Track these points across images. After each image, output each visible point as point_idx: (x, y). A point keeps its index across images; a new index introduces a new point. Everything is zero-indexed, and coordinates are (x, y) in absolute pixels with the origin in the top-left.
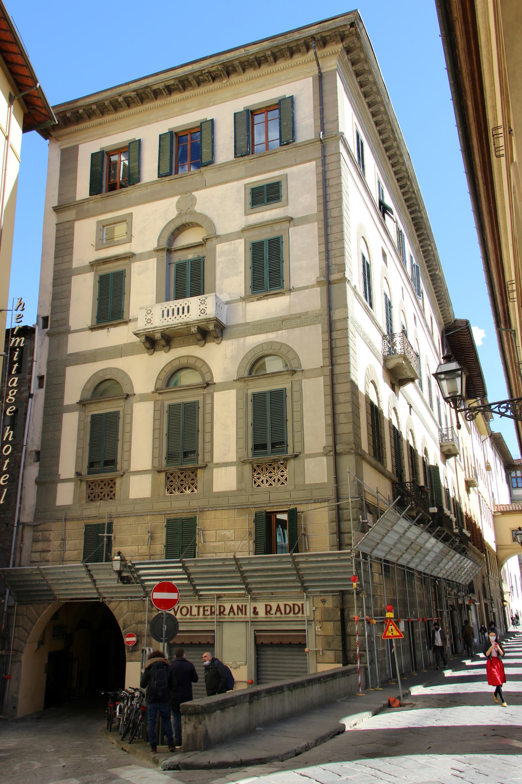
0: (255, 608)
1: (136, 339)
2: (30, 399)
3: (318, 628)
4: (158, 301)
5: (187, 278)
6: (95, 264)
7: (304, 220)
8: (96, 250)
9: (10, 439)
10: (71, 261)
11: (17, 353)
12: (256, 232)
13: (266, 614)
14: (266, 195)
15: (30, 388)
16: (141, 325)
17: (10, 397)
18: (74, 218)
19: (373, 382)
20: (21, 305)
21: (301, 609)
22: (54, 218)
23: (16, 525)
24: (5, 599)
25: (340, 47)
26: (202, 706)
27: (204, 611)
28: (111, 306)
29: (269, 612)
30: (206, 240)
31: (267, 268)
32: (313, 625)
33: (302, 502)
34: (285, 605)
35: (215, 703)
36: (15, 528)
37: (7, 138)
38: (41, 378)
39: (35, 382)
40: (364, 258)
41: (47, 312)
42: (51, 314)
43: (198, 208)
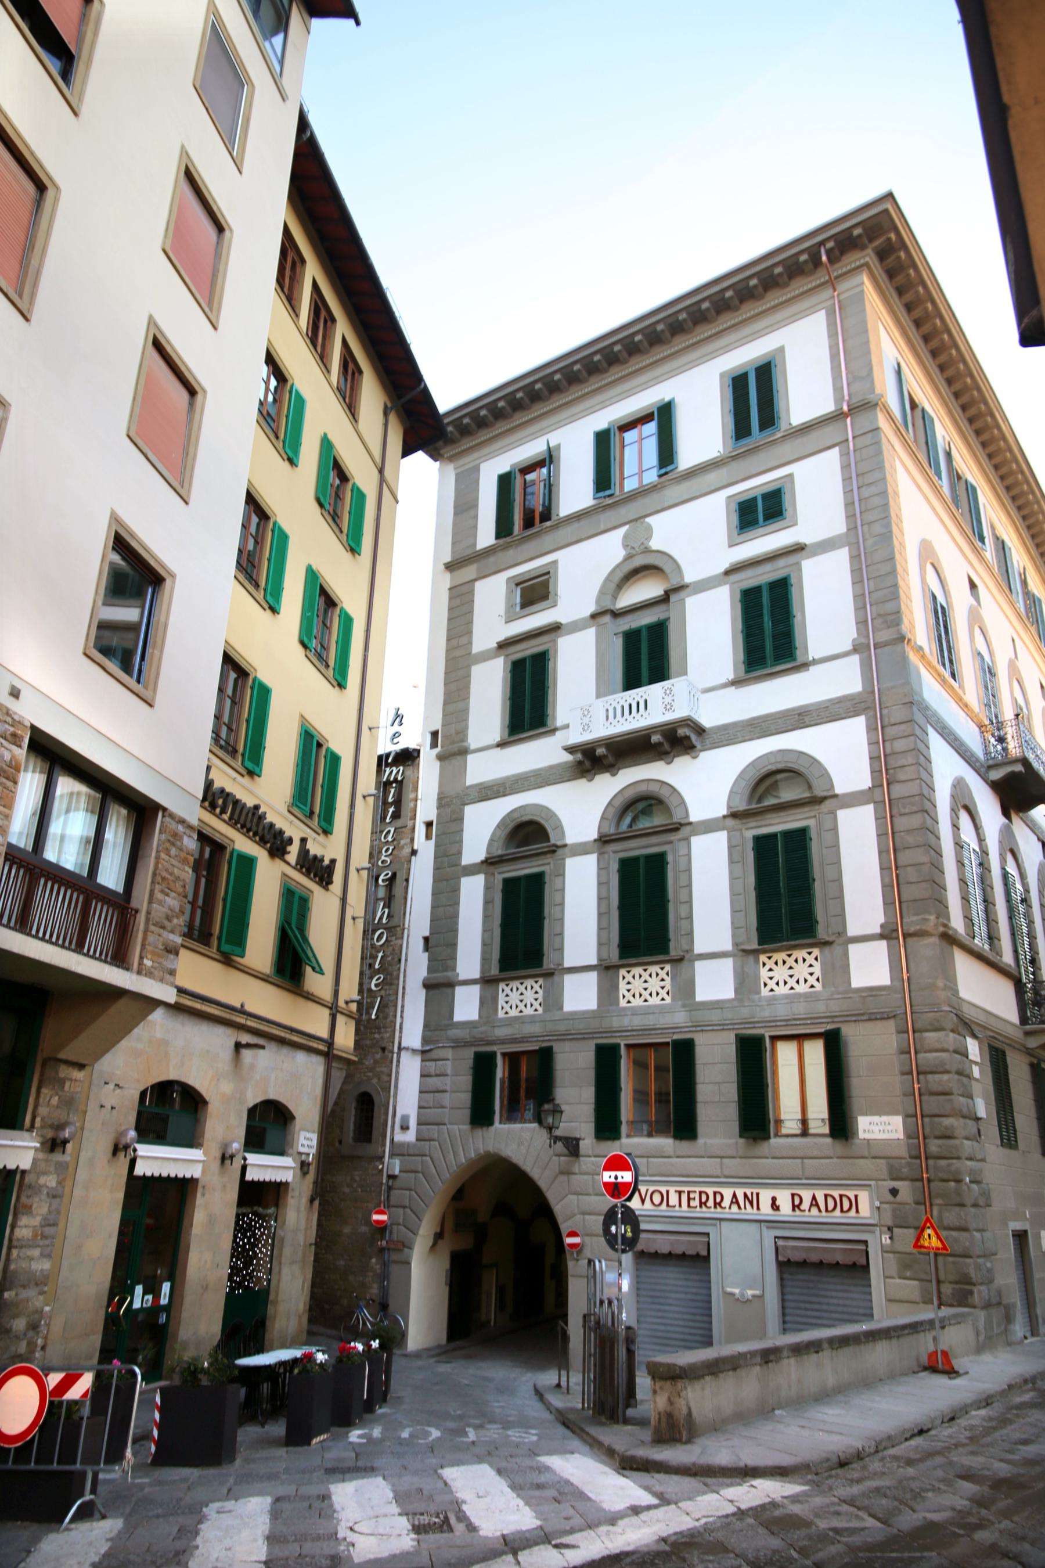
0: (774, 1199)
1: (568, 757)
2: (413, 858)
3: (886, 1239)
4: (598, 696)
5: (646, 655)
6: (503, 646)
7: (826, 546)
8: (506, 622)
9: (384, 921)
10: (470, 643)
11: (393, 791)
12: (749, 573)
13: (794, 1210)
14: (761, 510)
15: (412, 840)
16: (577, 736)
17: (383, 858)
18: (474, 577)
19: (966, 808)
20: (398, 717)
21: (854, 1204)
22: (446, 580)
23: (396, 1050)
24: (383, 1163)
25: (868, 256)
26: (680, 1367)
27: (689, 1199)
28: (529, 705)
29: (798, 1206)
30: (665, 599)
31: (769, 631)
32: (878, 1232)
33: (849, 1019)
34: (826, 1196)
35: (703, 1362)
36: (395, 1055)
37: (381, 471)
38: (429, 825)
39: (420, 831)
40: (934, 597)
41: (437, 725)
42: (443, 726)
43: (655, 544)
